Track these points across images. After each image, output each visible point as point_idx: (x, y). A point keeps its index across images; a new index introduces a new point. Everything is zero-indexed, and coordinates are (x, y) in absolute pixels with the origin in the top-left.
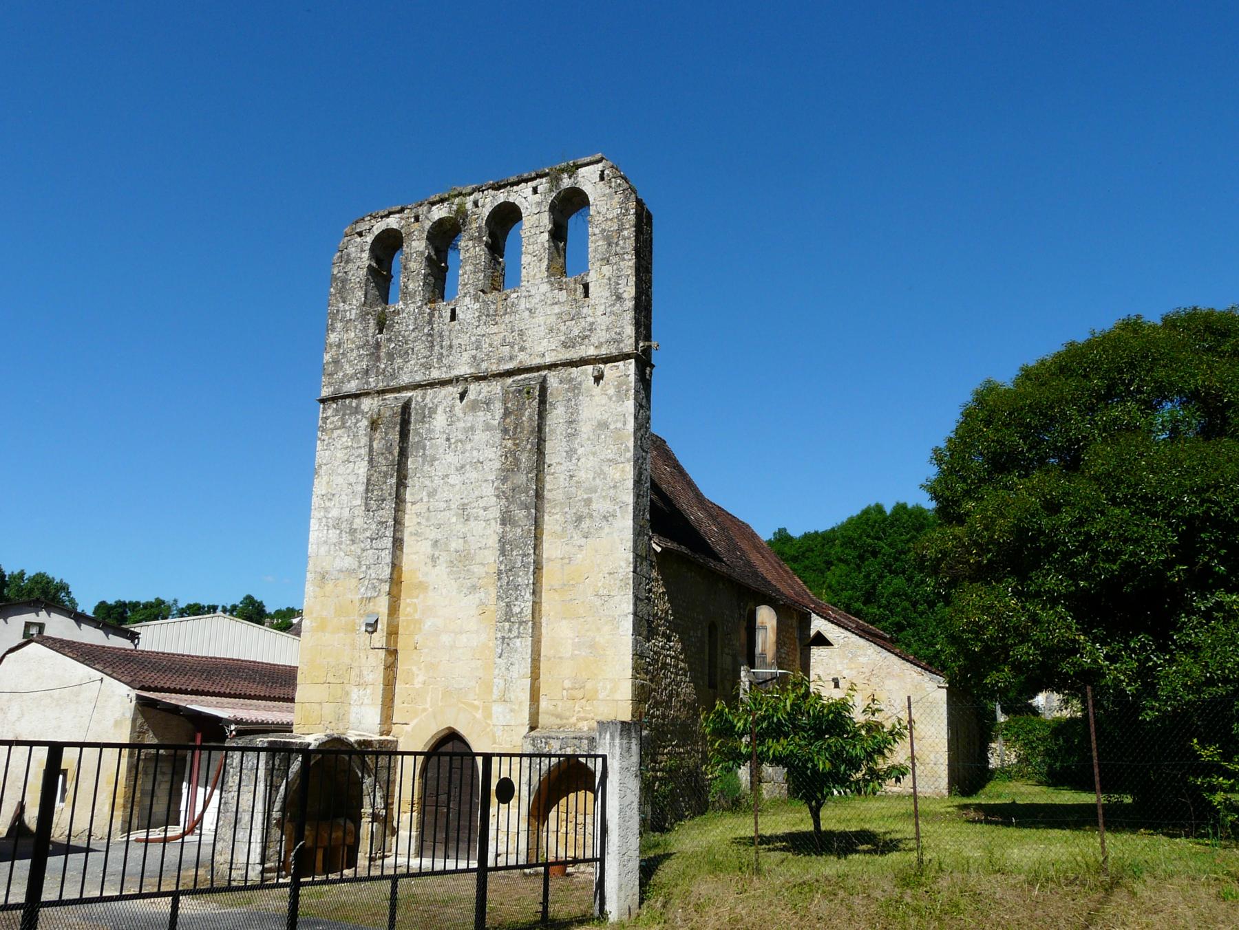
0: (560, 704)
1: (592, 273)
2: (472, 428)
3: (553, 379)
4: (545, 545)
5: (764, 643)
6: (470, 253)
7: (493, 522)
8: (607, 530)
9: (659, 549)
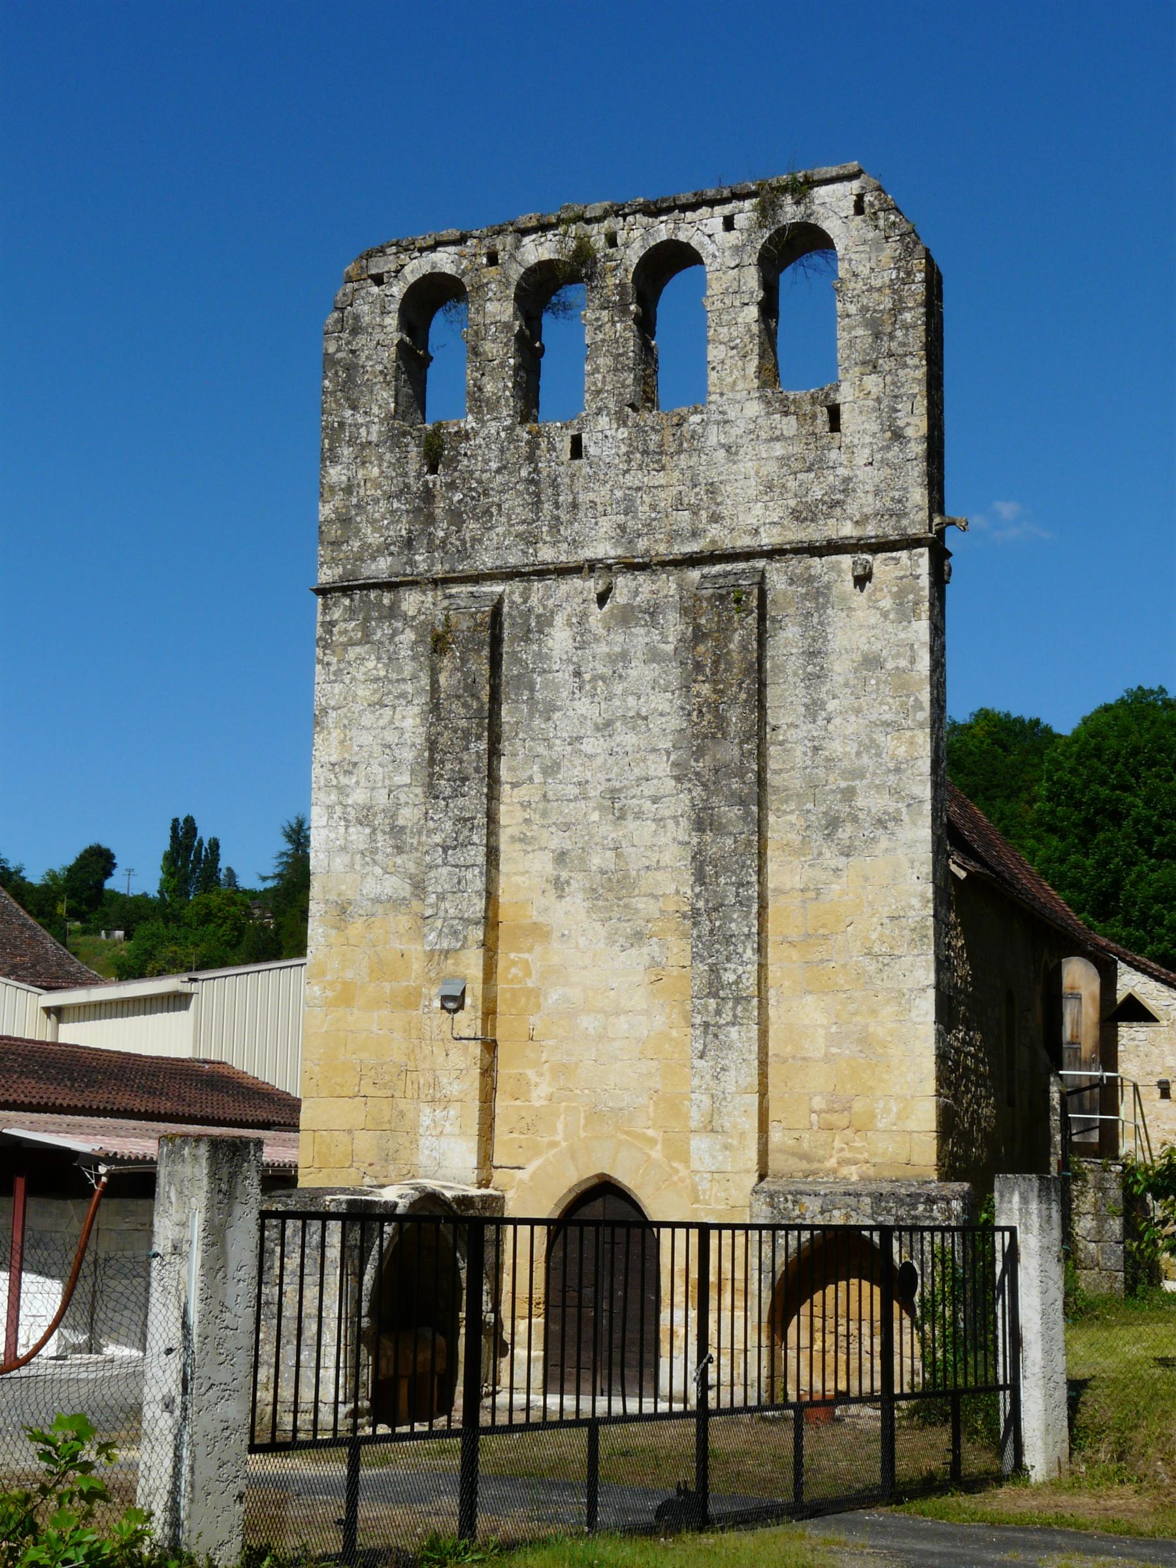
0: (806, 1136)
1: (845, 387)
2: (624, 657)
3: (777, 576)
4: (771, 867)
5: (1076, 1023)
6: (597, 329)
7: (670, 824)
8: (884, 843)
9: (962, 874)
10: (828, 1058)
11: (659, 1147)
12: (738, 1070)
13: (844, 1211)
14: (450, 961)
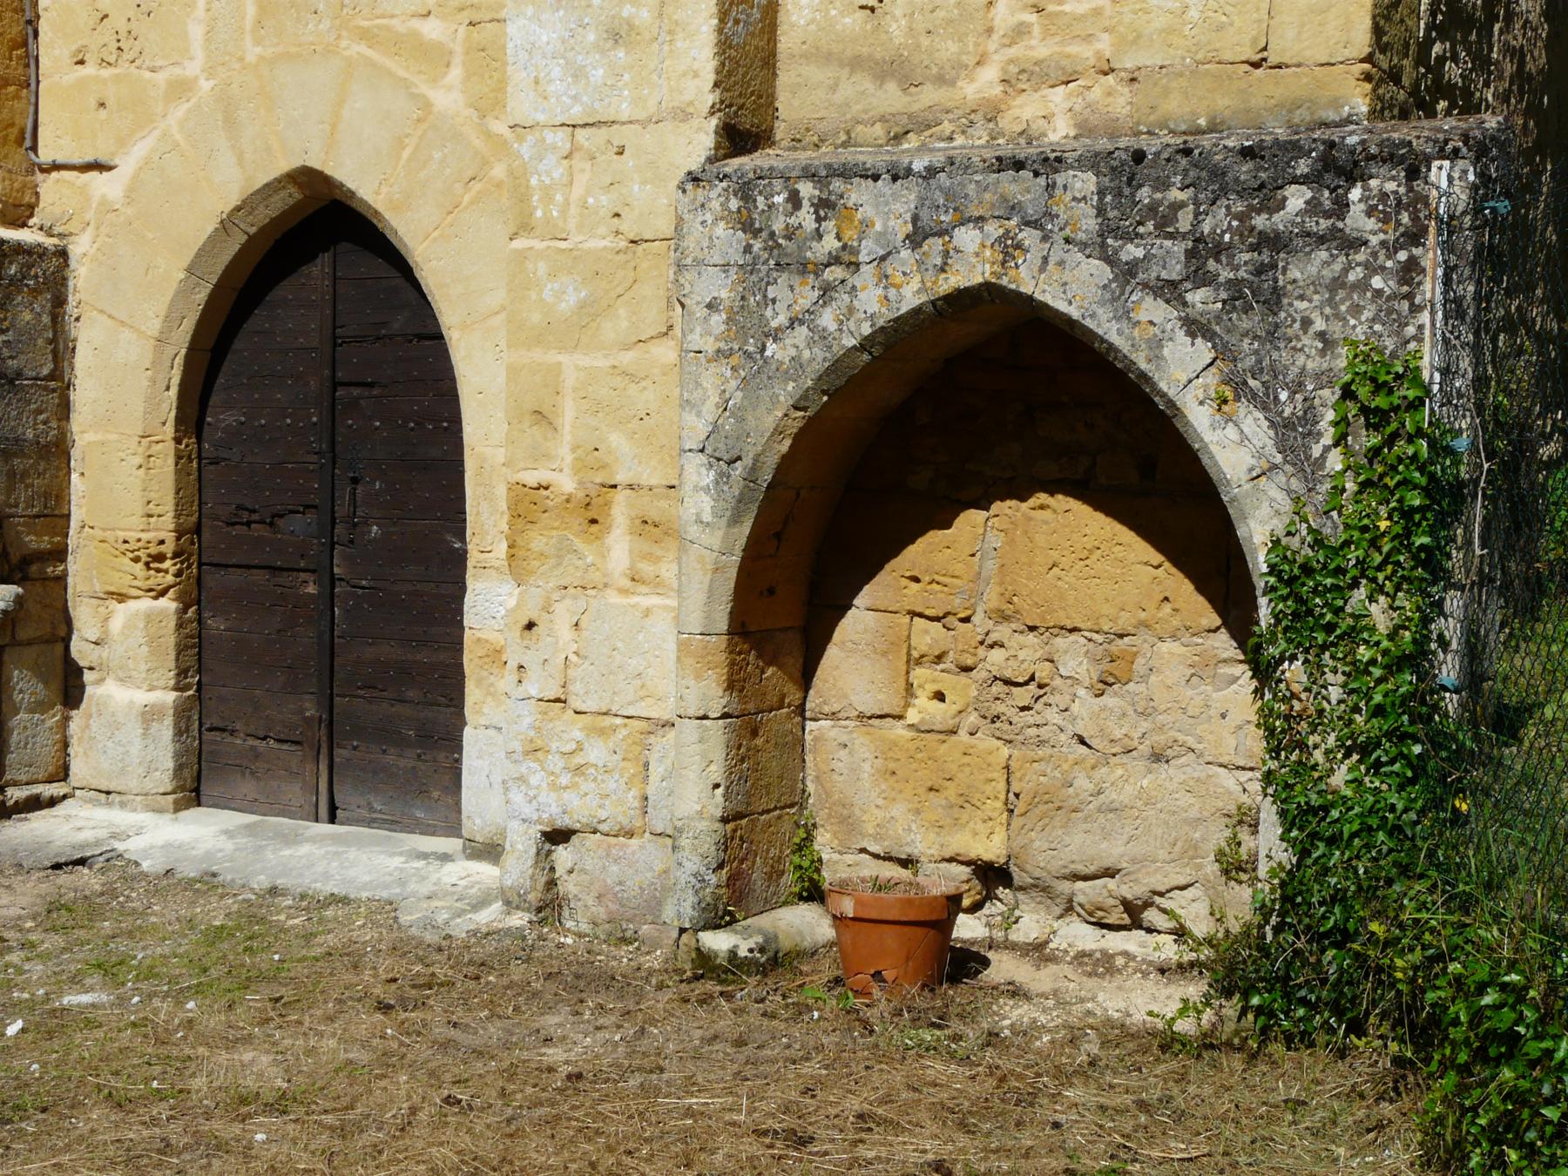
11: (456, 73)
13: (993, 229)
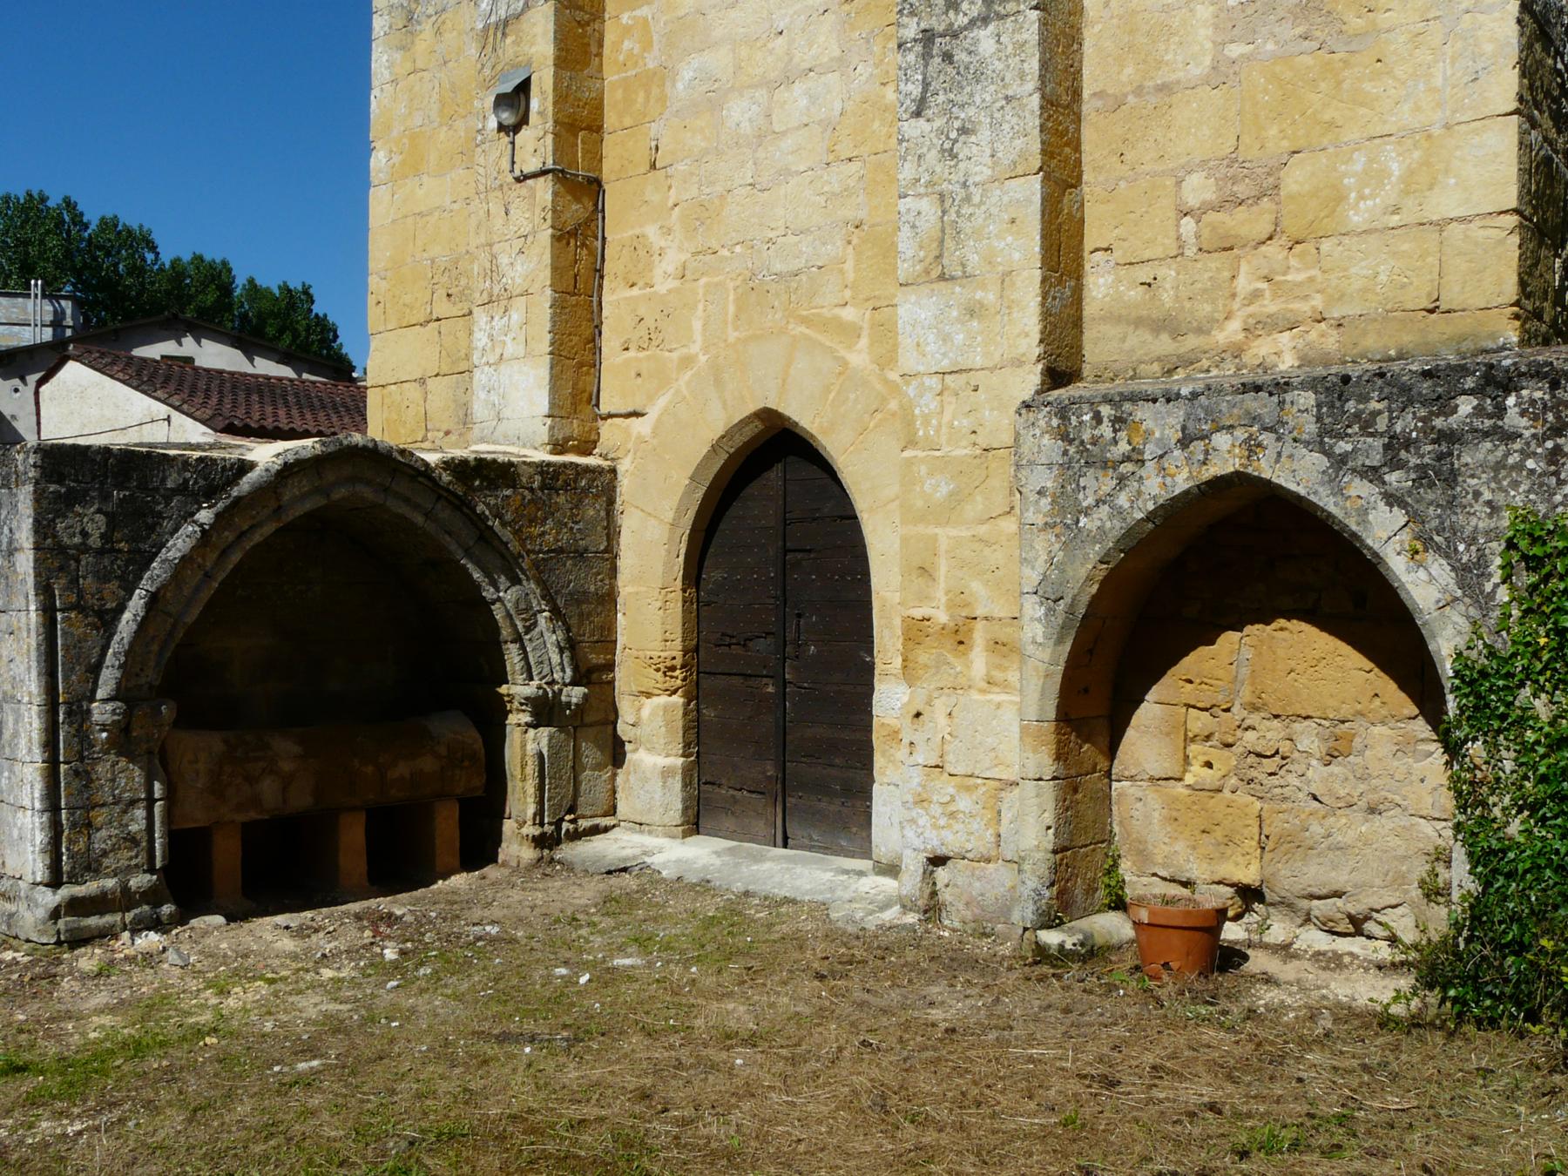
0: (1168, 273)
10: (1221, 75)
11: (864, 342)
12: (995, 125)
13: (1241, 434)
14: (509, 40)
